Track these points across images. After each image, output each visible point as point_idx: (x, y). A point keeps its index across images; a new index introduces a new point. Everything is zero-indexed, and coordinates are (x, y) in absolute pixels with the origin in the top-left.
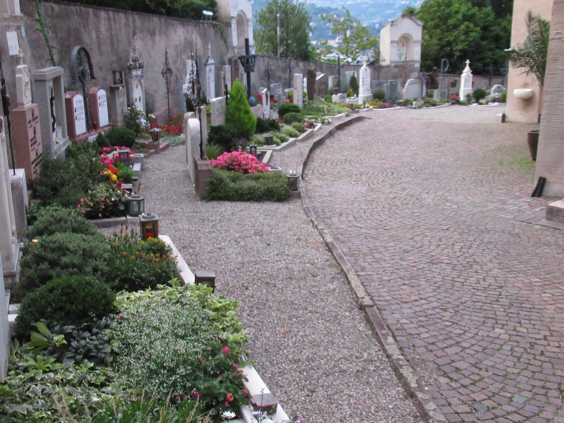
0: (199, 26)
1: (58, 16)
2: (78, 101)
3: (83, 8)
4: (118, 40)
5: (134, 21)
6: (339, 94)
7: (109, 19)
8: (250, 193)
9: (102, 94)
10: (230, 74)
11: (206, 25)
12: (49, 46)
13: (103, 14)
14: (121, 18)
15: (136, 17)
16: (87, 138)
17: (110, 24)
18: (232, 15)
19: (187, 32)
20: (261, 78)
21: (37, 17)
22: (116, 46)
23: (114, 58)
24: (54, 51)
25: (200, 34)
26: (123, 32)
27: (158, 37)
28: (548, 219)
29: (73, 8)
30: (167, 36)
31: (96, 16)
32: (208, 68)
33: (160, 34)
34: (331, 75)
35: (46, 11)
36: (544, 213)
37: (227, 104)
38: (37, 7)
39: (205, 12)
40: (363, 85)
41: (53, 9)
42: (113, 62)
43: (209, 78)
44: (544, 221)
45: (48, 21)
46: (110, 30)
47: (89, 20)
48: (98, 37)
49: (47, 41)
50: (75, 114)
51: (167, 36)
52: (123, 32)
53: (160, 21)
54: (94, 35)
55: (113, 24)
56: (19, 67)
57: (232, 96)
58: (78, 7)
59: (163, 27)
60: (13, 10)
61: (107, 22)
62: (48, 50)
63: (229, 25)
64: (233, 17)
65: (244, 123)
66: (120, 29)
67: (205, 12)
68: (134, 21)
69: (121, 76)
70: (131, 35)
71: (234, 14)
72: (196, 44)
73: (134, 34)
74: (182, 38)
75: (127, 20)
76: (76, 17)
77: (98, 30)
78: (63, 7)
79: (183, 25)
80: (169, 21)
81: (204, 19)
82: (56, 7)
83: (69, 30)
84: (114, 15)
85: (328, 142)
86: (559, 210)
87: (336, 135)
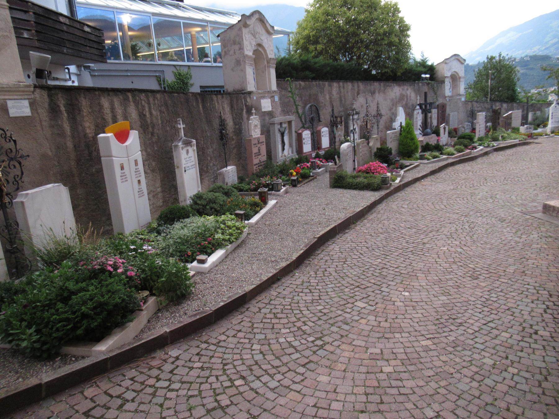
0: (414, 85)
1: (303, 88)
2: (307, 135)
3: (321, 82)
4: (345, 99)
5: (358, 87)
6: (526, 126)
7: (339, 87)
8: (356, 185)
9: (325, 131)
10: (436, 115)
11: (420, 84)
12: (296, 105)
13: (335, 84)
14: (349, 85)
15: (360, 84)
16: (311, 154)
17: (340, 90)
18: (446, 75)
19: (403, 89)
20: (468, 117)
21: (289, 90)
22: (343, 102)
23: (342, 109)
24: (299, 107)
25: (415, 91)
26: (349, 94)
27: (377, 94)
28: (544, 213)
29: (314, 83)
30: (384, 93)
31: (330, 86)
32: (415, 112)
33: (379, 93)
34: (532, 111)
35: (296, 86)
36: (540, 208)
37: (400, 134)
38: (290, 85)
39: (423, 76)
40: (552, 118)
41: (300, 84)
42: (340, 112)
43: (417, 118)
44: (540, 215)
45: (297, 92)
46: (339, 93)
47: (325, 89)
48: (330, 98)
49: (41, 121)
50: (304, 141)
51: (384, 93)
52: (349, 94)
53: (380, 85)
54: (327, 97)
55: (342, 90)
56: (252, 117)
57: (404, 130)
58: (317, 82)
59: (382, 88)
60: (270, 88)
61: (337, 89)
62: (295, 107)
63: (443, 82)
64: (446, 77)
65: (410, 146)
66: (348, 92)
67: (423, 76)
68: (358, 87)
69: (341, 119)
70: (356, 95)
71: (448, 74)
72: (410, 97)
73: (358, 94)
74: (398, 94)
75: (353, 86)
76: (315, 88)
77: (330, 93)
78: (307, 83)
79: (400, 86)
80: (387, 84)
81: (423, 80)
82: (302, 83)
83: (310, 95)
84: (343, 84)
85: (479, 160)
86: (554, 208)
87: (491, 155)
